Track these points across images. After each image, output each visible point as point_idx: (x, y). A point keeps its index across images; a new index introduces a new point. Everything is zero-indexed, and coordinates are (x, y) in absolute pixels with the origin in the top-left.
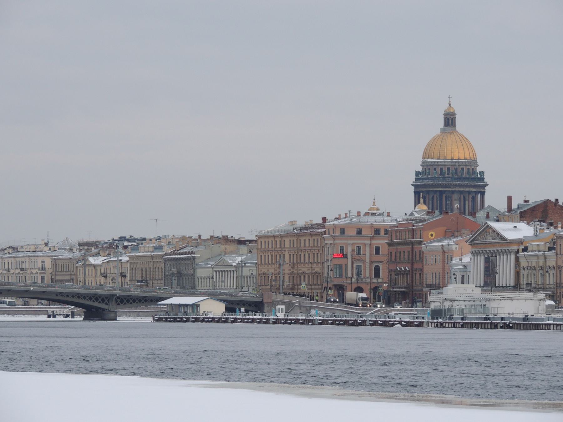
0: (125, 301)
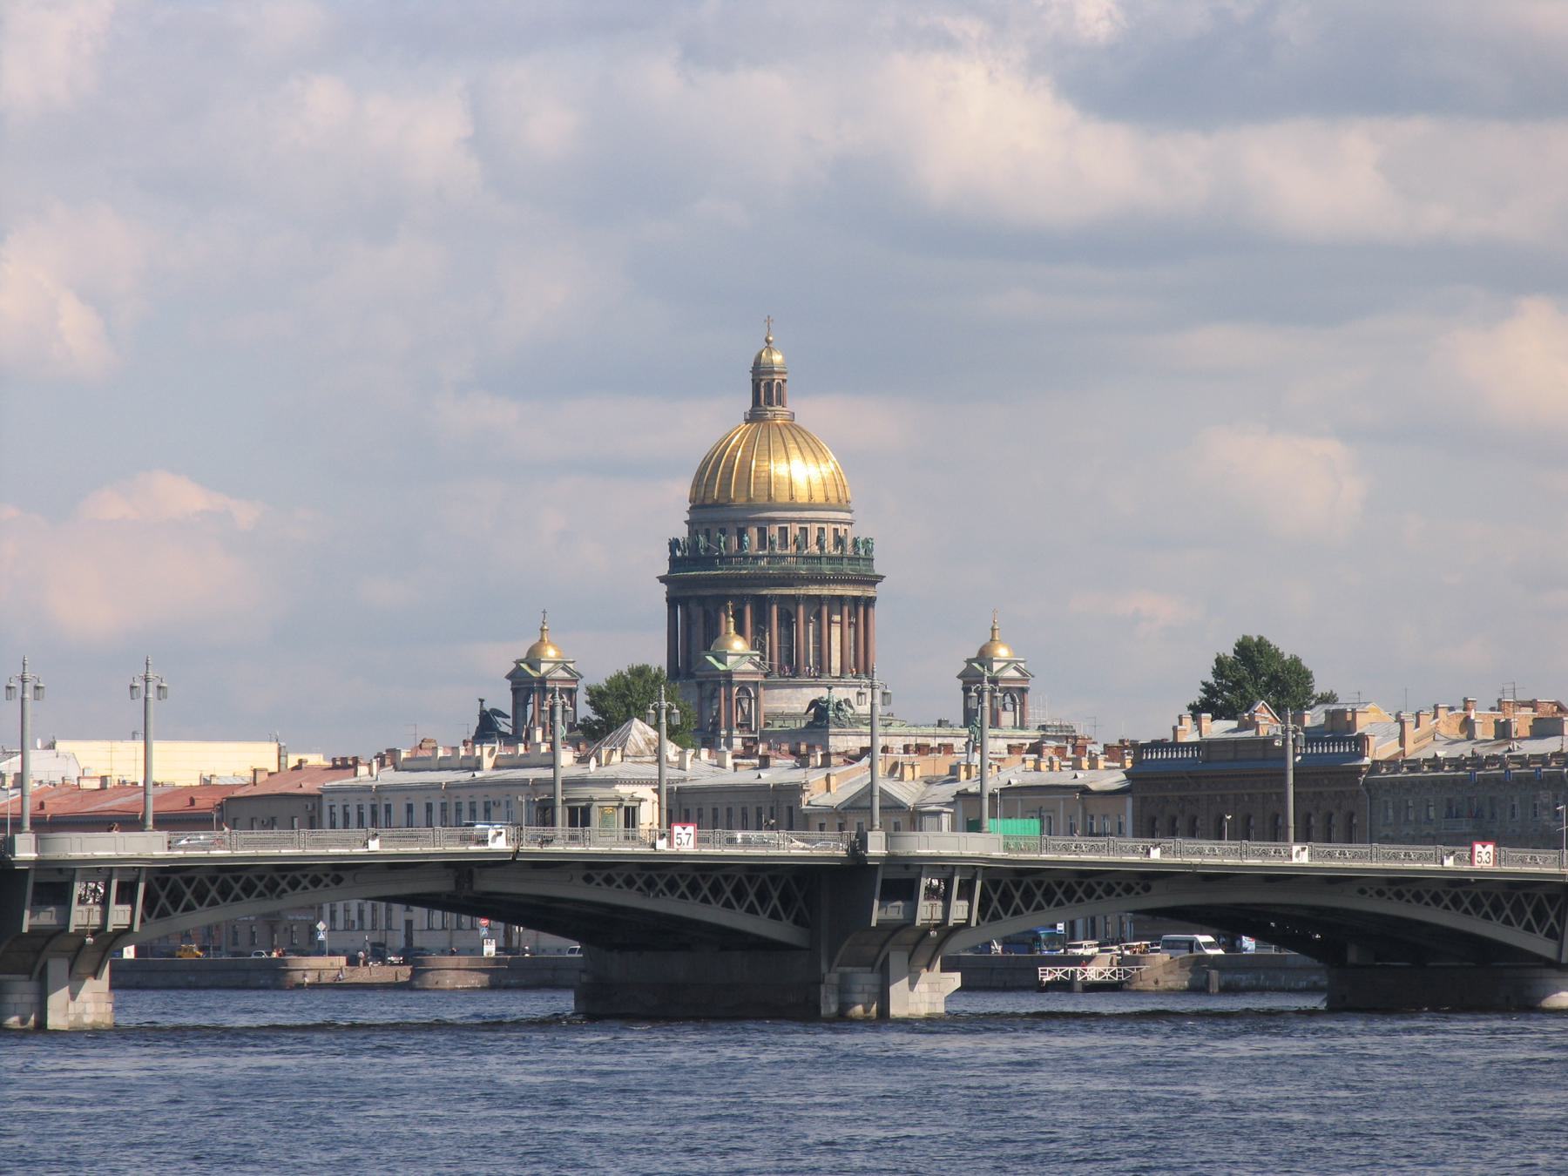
0: (1059, 895)
